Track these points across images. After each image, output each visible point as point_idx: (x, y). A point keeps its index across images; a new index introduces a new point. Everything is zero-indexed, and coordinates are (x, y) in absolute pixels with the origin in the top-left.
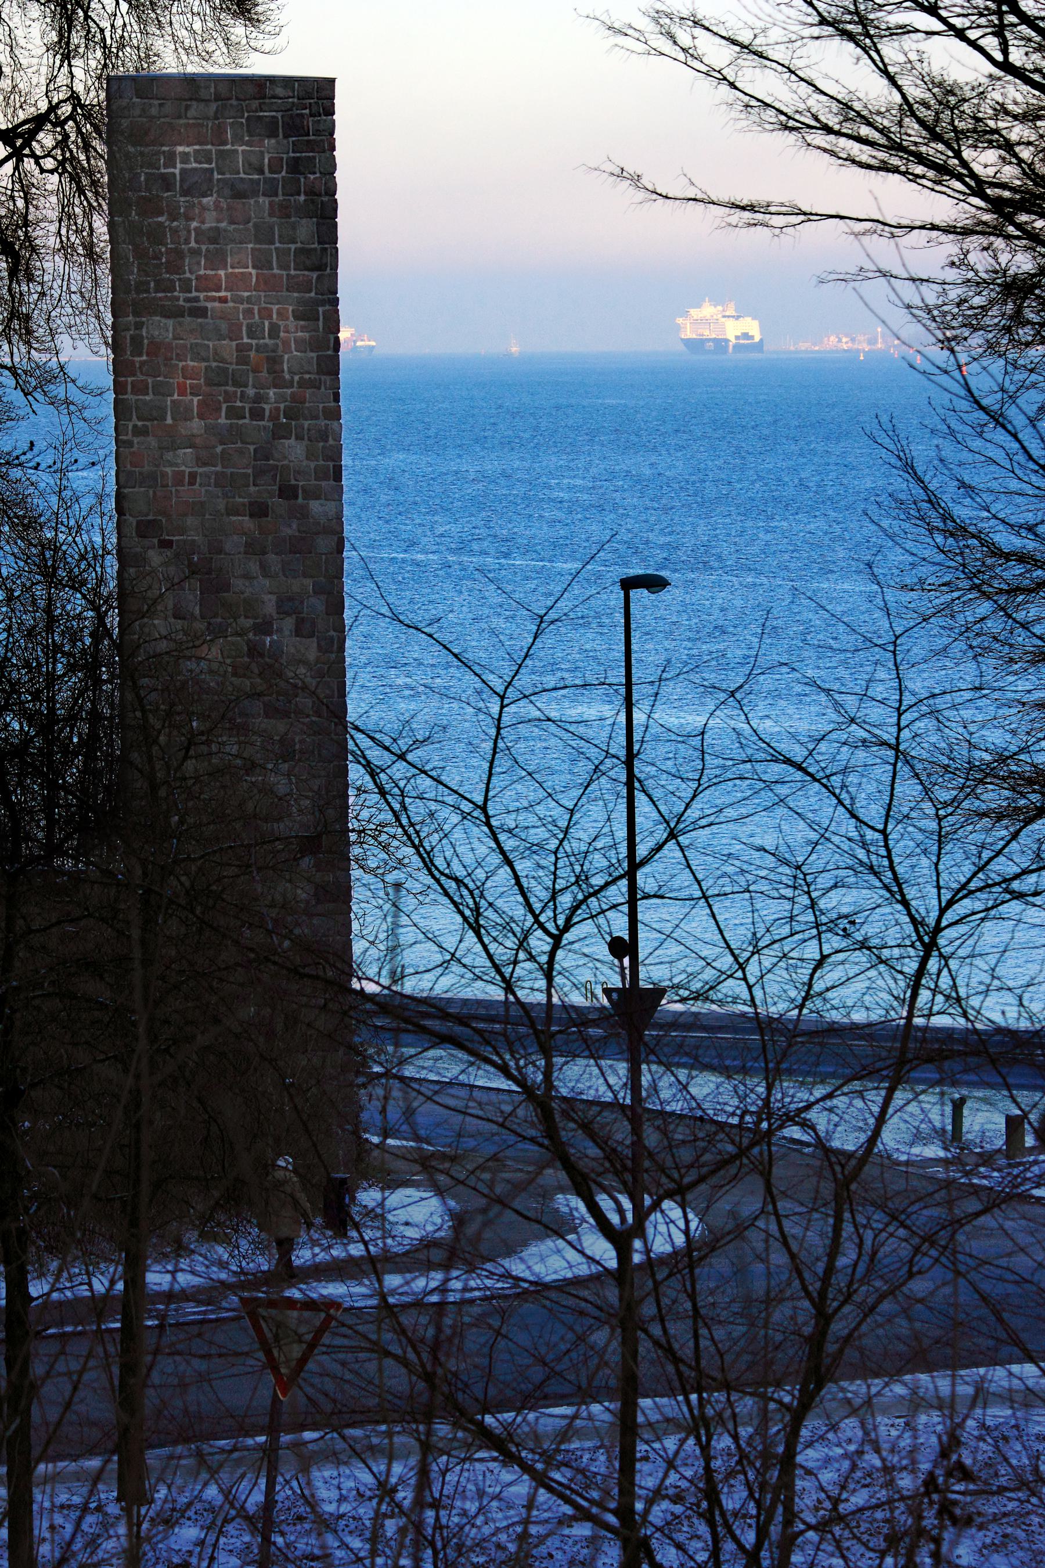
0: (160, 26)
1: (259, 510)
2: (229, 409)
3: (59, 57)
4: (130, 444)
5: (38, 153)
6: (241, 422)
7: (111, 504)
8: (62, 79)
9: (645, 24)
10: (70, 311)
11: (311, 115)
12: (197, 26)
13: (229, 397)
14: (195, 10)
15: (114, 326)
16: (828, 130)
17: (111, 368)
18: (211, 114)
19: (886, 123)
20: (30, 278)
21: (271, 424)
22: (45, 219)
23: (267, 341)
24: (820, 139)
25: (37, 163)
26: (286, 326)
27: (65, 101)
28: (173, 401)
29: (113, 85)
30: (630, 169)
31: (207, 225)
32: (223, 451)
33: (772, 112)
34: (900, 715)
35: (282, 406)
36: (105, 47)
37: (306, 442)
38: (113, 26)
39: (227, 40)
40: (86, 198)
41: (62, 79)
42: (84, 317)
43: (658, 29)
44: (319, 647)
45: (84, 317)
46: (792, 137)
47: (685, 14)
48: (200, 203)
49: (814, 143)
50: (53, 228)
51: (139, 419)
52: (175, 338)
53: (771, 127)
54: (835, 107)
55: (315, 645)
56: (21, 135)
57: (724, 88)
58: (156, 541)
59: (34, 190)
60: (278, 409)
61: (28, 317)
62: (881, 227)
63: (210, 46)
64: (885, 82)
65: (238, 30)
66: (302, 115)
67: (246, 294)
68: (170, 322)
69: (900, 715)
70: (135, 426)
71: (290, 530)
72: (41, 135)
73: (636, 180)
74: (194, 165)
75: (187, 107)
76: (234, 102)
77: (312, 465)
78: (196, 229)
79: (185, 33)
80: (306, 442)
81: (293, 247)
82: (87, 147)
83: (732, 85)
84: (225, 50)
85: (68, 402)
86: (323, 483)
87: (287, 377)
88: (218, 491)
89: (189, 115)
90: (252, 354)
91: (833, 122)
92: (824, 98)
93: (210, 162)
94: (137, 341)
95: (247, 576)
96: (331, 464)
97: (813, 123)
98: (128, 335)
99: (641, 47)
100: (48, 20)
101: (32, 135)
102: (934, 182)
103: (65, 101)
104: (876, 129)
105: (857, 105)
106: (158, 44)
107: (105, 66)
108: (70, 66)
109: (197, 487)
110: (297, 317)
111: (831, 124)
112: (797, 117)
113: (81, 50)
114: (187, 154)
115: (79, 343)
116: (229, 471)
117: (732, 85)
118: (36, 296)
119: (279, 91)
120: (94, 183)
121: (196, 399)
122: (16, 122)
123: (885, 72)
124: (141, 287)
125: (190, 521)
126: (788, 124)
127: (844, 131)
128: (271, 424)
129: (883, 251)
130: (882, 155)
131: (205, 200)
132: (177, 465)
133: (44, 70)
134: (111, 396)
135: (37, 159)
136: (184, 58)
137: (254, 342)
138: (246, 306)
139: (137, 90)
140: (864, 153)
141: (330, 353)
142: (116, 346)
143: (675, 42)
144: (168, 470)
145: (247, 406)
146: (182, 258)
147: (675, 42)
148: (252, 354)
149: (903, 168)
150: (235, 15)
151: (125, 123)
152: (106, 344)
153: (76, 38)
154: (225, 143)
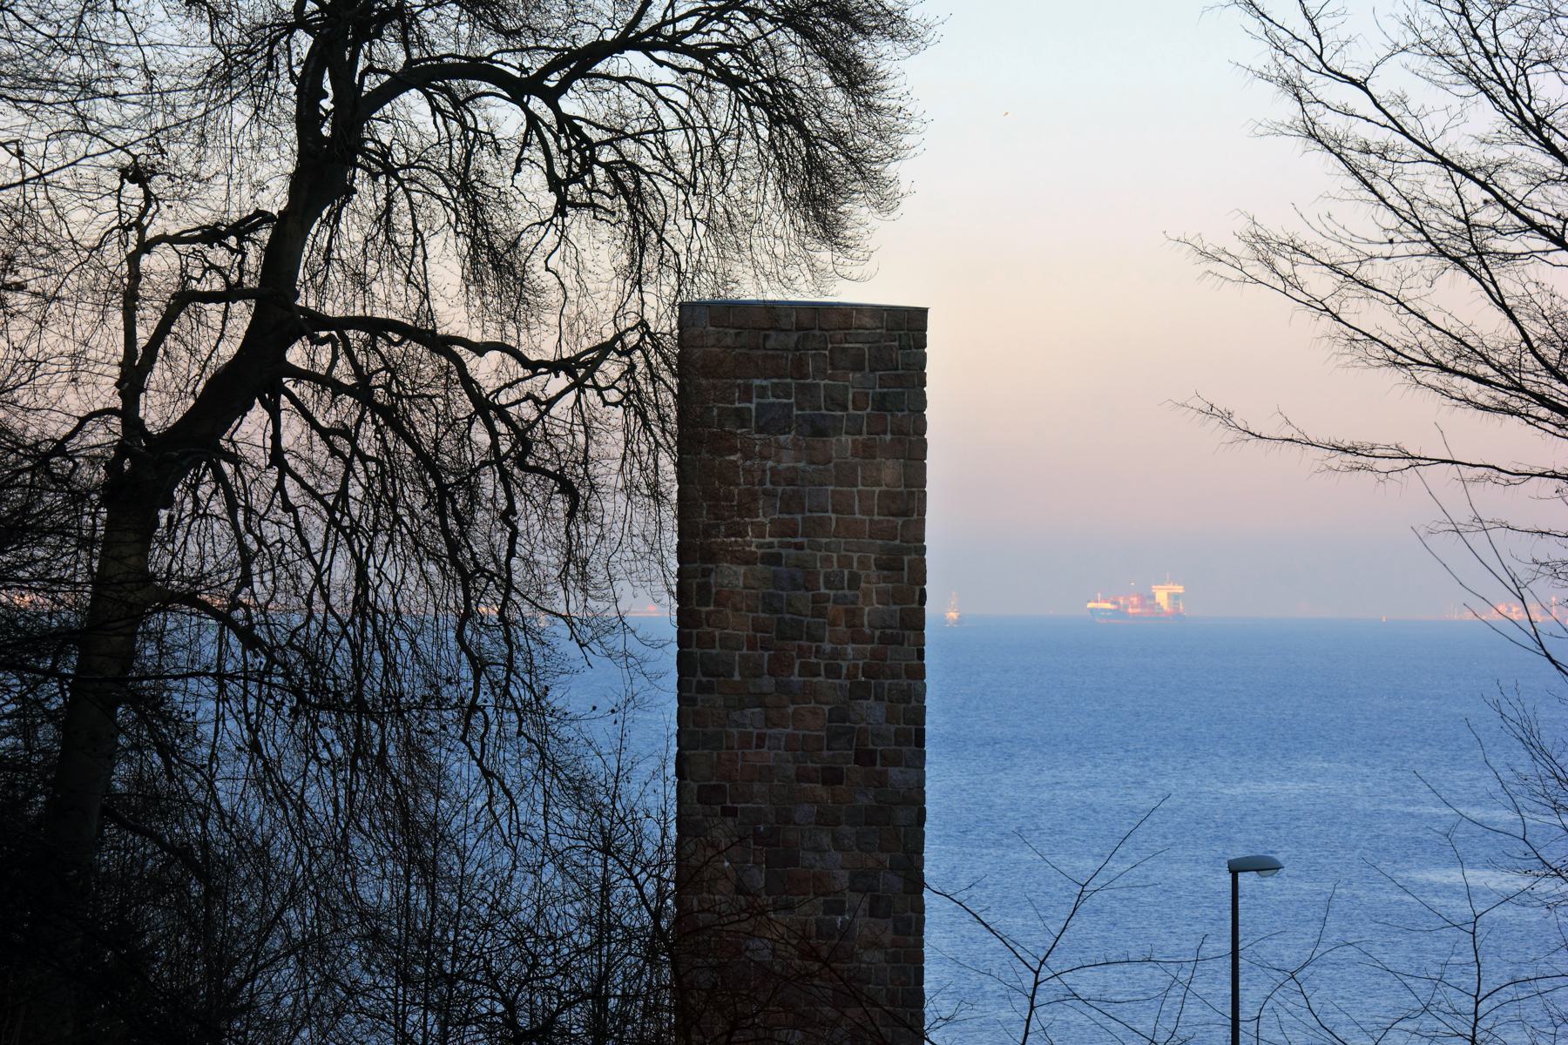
0: (739, 250)
1: (832, 777)
2: (802, 665)
3: (629, 282)
4: (693, 701)
5: (602, 385)
6: (815, 680)
7: (671, 770)
8: (633, 305)
9: (1238, 248)
10: (631, 555)
11: (901, 348)
12: (779, 250)
13: (802, 652)
14: (778, 233)
15: (680, 573)
16: (1443, 368)
17: (675, 618)
18: (792, 344)
19: (1503, 360)
20: (587, 520)
21: (847, 683)
22: (608, 457)
23: (846, 592)
24: (1432, 376)
25: (600, 394)
26: (868, 576)
27: (632, 329)
28: (741, 656)
29: (688, 312)
30: (1220, 405)
31: (784, 465)
32: (795, 711)
33: (1378, 347)
34: (1477, 1003)
35: (861, 663)
36: (679, 272)
37: (886, 703)
38: (688, 249)
39: (812, 267)
40: (653, 435)
41: (633, 305)
42: (646, 563)
43: (1254, 255)
44: (896, 931)
45: (646, 563)
46: (1399, 375)
47: (1284, 238)
48: (777, 441)
49: (1424, 381)
50: (616, 465)
51: (704, 674)
52: (745, 587)
53: (1378, 363)
54: (1448, 343)
55: (891, 926)
56: (584, 365)
57: (1326, 320)
58: (718, 808)
59: (596, 424)
60: (856, 666)
61: (586, 561)
62: (1496, 472)
63: (792, 272)
64: (1503, 315)
65: (824, 255)
66: (891, 347)
67: (824, 540)
68: (742, 569)
69: (1477, 1003)
70: (699, 682)
71: (865, 800)
72: (605, 365)
73: (1226, 417)
74: (772, 400)
75: (766, 337)
76: (817, 332)
77: (893, 728)
78: (771, 469)
79: (766, 257)
80: (886, 703)
81: (877, 490)
82: (654, 378)
83: (1336, 317)
84: (809, 277)
85: (626, 655)
86: (904, 749)
87: (867, 631)
88: (789, 755)
89: (768, 345)
90: (830, 605)
91: (1447, 360)
92: (1435, 332)
93: (788, 396)
94: (704, 588)
95: (818, 849)
96: (913, 728)
97: (1427, 360)
98: (694, 583)
99: (1235, 274)
100: (619, 243)
101: (593, 366)
102: (1559, 426)
103: (632, 329)
104: (1493, 366)
105: (1470, 341)
106: (738, 270)
107: (679, 291)
108: (641, 291)
109: (764, 750)
110: (879, 567)
111: (1443, 361)
112: (1407, 352)
113: (654, 275)
114: (764, 388)
115: (640, 591)
116: (801, 733)
117: (1336, 317)
118: (594, 539)
119: (867, 321)
120: (662, 419)
121: (766, 654)
122: (579, 350)
123: (1503, 306)
124: (707, 532)
125: (756, 786)
126: (1398, 359)
127: (1459, 368)
128: (847, 683)
129: (1494, 500)
130: (1502, 396)
131: (782, 438)
132: (744, 725)
133: (613, 296)
134: (674, 648)
135: (600, 390)
136: (765, 285)
137: (832, 593)
138: (824, 553)
139: (711, 318)
140: (1483, 394)
141: (915, 606)
142: (682, 595)
143: (1273, 270)
144: (735, 731)
145: (823, 663)
146: (756, 500)
147: (1273, 270)
148: (830, 605)
149: (1524, 411)
150: (822, 240)
151: (698, 353)
152: (670, 592)
153: (649, 262)
154: (806, 376)
